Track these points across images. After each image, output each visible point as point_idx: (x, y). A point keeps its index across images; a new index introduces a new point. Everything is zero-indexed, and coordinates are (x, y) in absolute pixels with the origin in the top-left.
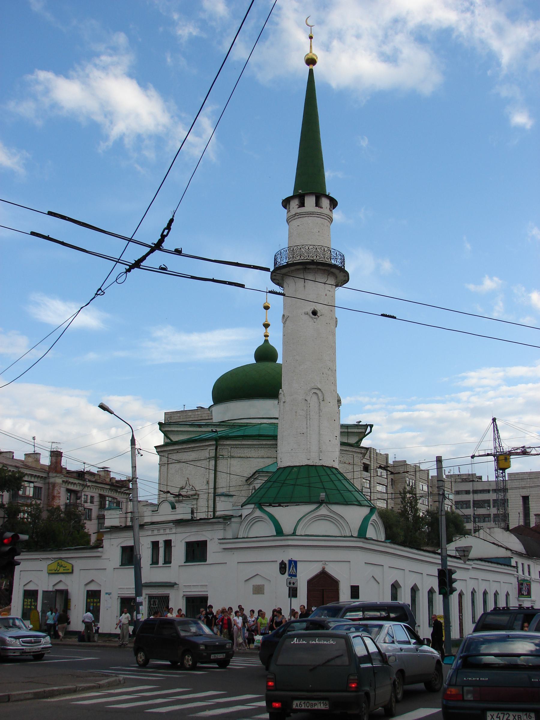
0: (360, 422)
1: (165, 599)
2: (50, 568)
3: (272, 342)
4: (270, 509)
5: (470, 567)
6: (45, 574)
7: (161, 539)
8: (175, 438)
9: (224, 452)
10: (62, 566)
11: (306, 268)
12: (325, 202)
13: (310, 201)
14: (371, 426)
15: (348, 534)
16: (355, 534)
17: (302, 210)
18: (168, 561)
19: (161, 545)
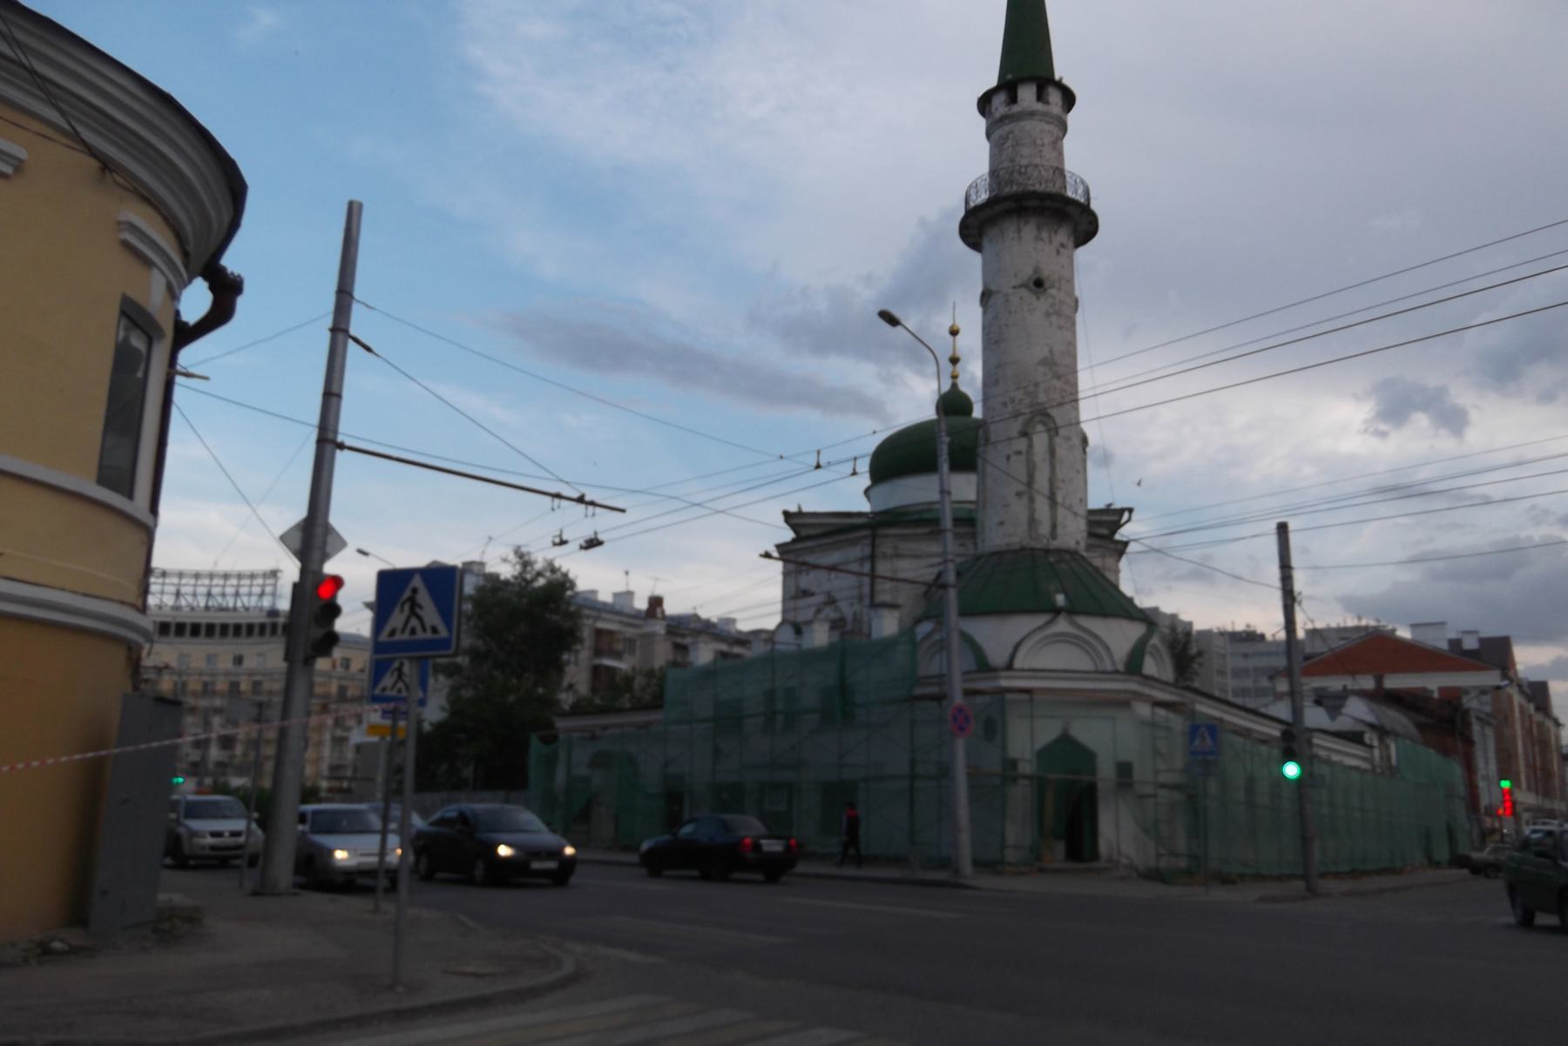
3: (963, 388)
8: (804, 532)
9: (886, 547)
12: (1054, 96)
13: (1027, 94)
14: (1131, 510)
15: (1109, 667)
16: (1121, 667)
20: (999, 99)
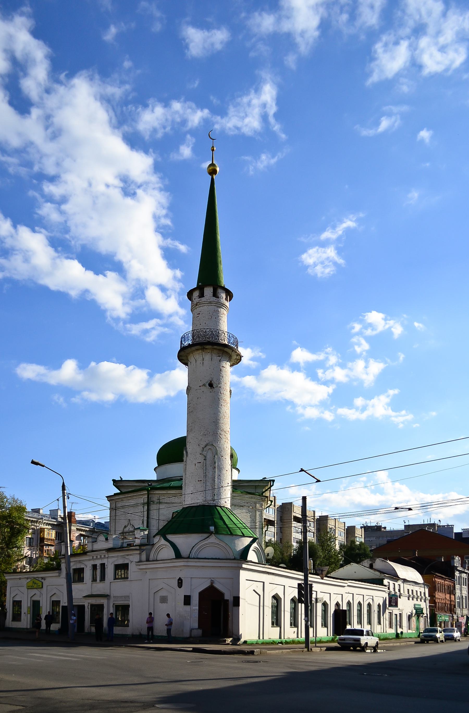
0: (265, 478)
1: (101, 607)
2: (28, 585)
4: (170, 537)
5: (346, 585)
6: (24, 589)
7: (98, 562)
8: (124, 490)
10: (35, 583)
11: (204, 348)
13: (208, 291)
14: (273, 481)
18: (103, 578)
19: (98, 567)
20: (196, 294)
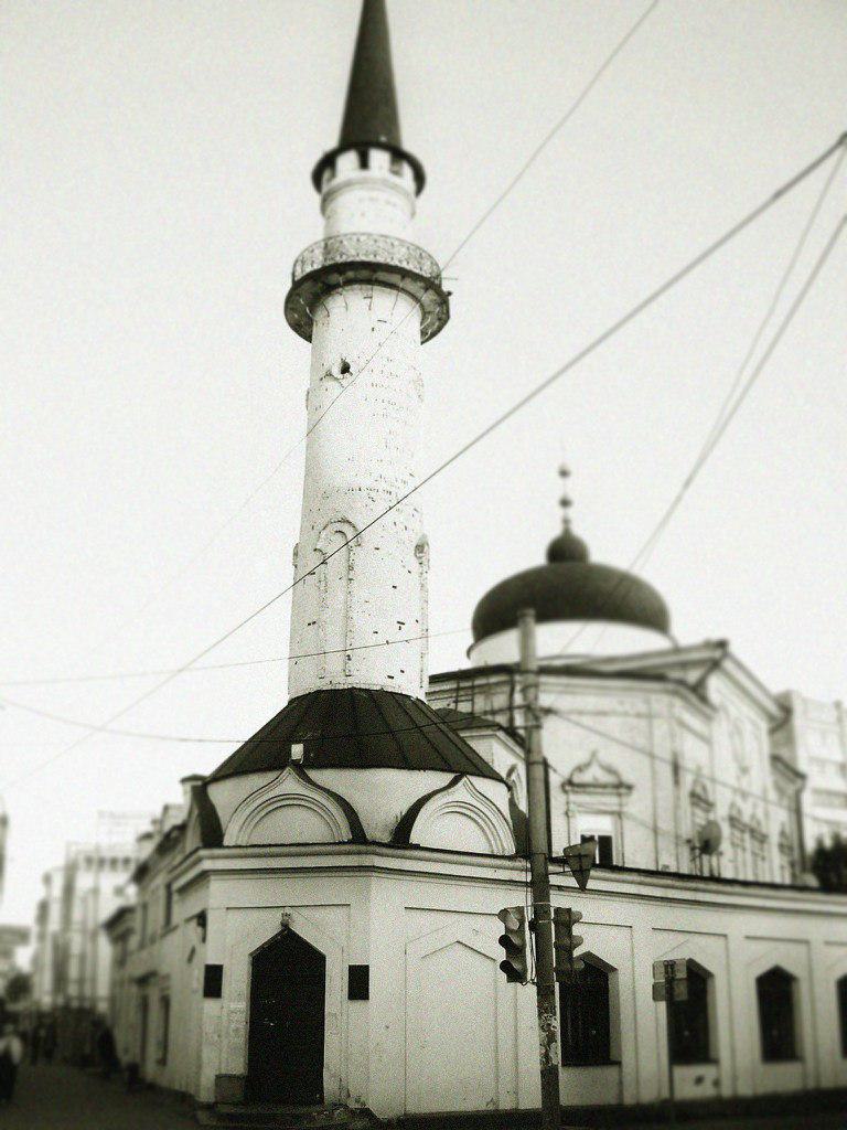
17: (364, 174)
